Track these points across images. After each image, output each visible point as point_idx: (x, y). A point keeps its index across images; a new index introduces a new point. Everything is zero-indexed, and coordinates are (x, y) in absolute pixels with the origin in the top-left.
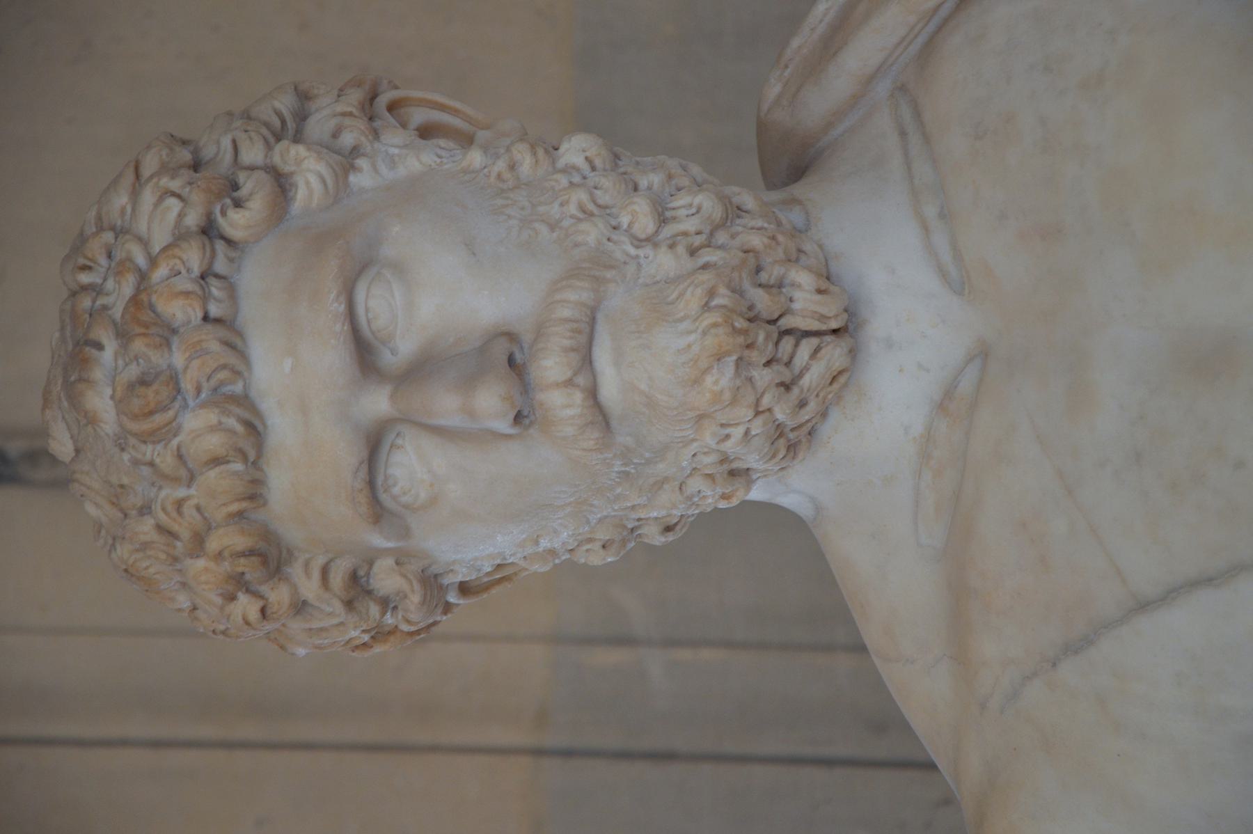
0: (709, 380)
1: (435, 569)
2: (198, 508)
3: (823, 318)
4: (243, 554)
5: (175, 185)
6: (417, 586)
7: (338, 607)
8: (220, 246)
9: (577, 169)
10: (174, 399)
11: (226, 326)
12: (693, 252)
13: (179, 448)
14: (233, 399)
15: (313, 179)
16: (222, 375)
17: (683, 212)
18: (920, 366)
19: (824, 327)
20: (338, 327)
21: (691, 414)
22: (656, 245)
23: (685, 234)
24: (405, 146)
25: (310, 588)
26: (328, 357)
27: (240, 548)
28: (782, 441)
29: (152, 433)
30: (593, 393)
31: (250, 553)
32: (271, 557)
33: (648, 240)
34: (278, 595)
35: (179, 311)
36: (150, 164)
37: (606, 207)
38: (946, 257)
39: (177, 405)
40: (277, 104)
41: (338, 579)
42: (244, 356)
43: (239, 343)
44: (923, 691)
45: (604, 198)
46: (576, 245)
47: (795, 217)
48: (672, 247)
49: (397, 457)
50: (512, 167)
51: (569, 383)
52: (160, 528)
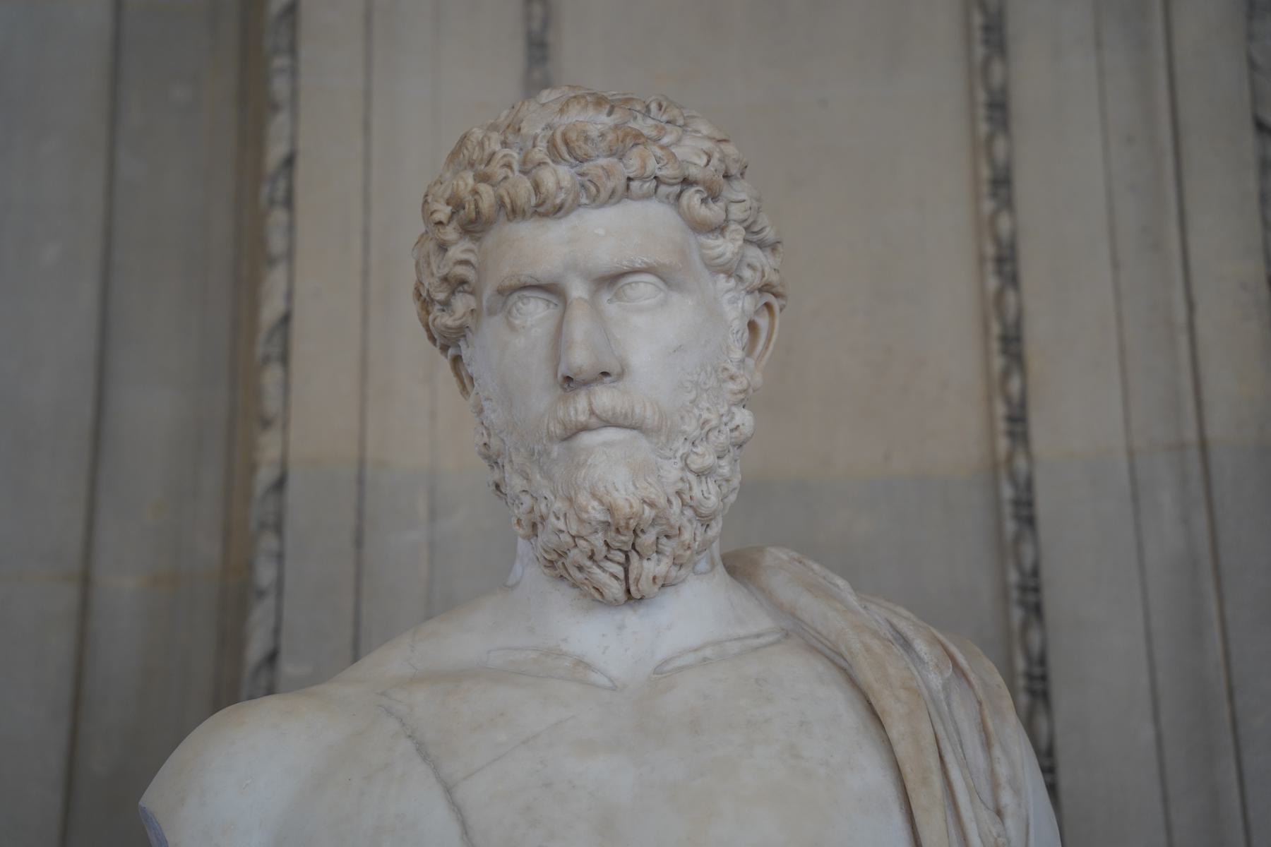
0: (595, 504)
1: (469, 335)
2: (506, 178)
3: (637, 581)
4: (477, 207)
5: (714, 161)
6: (458, 323)
7: (444, 271)
8: (677, 189)
9: (732, 418)
10: (576, 159)
11: (625, 192)
12: (679, 493)
13: (545, 163)
14: (577, 197)
15: (720, 250)
16: (593, 189)
17: (705, 488)
18: (606, 648)
19: (631, 581)
20: (625, 263)
21: (573, 493)
22: (683, 469)
23: (691, 489)
24: (743, 311)
25: (456, 252)
26: (606, 257)
27: (480, 205)
28: (555, 557)
29: (555, 146)
30: (585, 428)
31: (478, 213)
32: (474, 227)
33: (686, 465)
34: (450, 233)
35: (633, 163)
36: (730, 149)
37: (707, 439)
38: (678, 663)
39: (572, 161)
40: (768, 230)
41: (461, 270)
42: (603, 205)
43: (613, 201)
44: (391, 661)
45: (712, 436)
46: (682, 418)
47: (703, 565)
48: (682, 479)
49: (541, 305)
50: (732, 378)
51: (592, 413)
52: (494, 154)
